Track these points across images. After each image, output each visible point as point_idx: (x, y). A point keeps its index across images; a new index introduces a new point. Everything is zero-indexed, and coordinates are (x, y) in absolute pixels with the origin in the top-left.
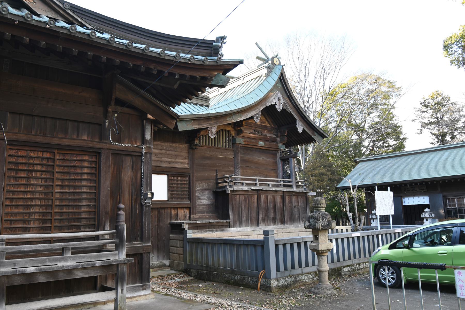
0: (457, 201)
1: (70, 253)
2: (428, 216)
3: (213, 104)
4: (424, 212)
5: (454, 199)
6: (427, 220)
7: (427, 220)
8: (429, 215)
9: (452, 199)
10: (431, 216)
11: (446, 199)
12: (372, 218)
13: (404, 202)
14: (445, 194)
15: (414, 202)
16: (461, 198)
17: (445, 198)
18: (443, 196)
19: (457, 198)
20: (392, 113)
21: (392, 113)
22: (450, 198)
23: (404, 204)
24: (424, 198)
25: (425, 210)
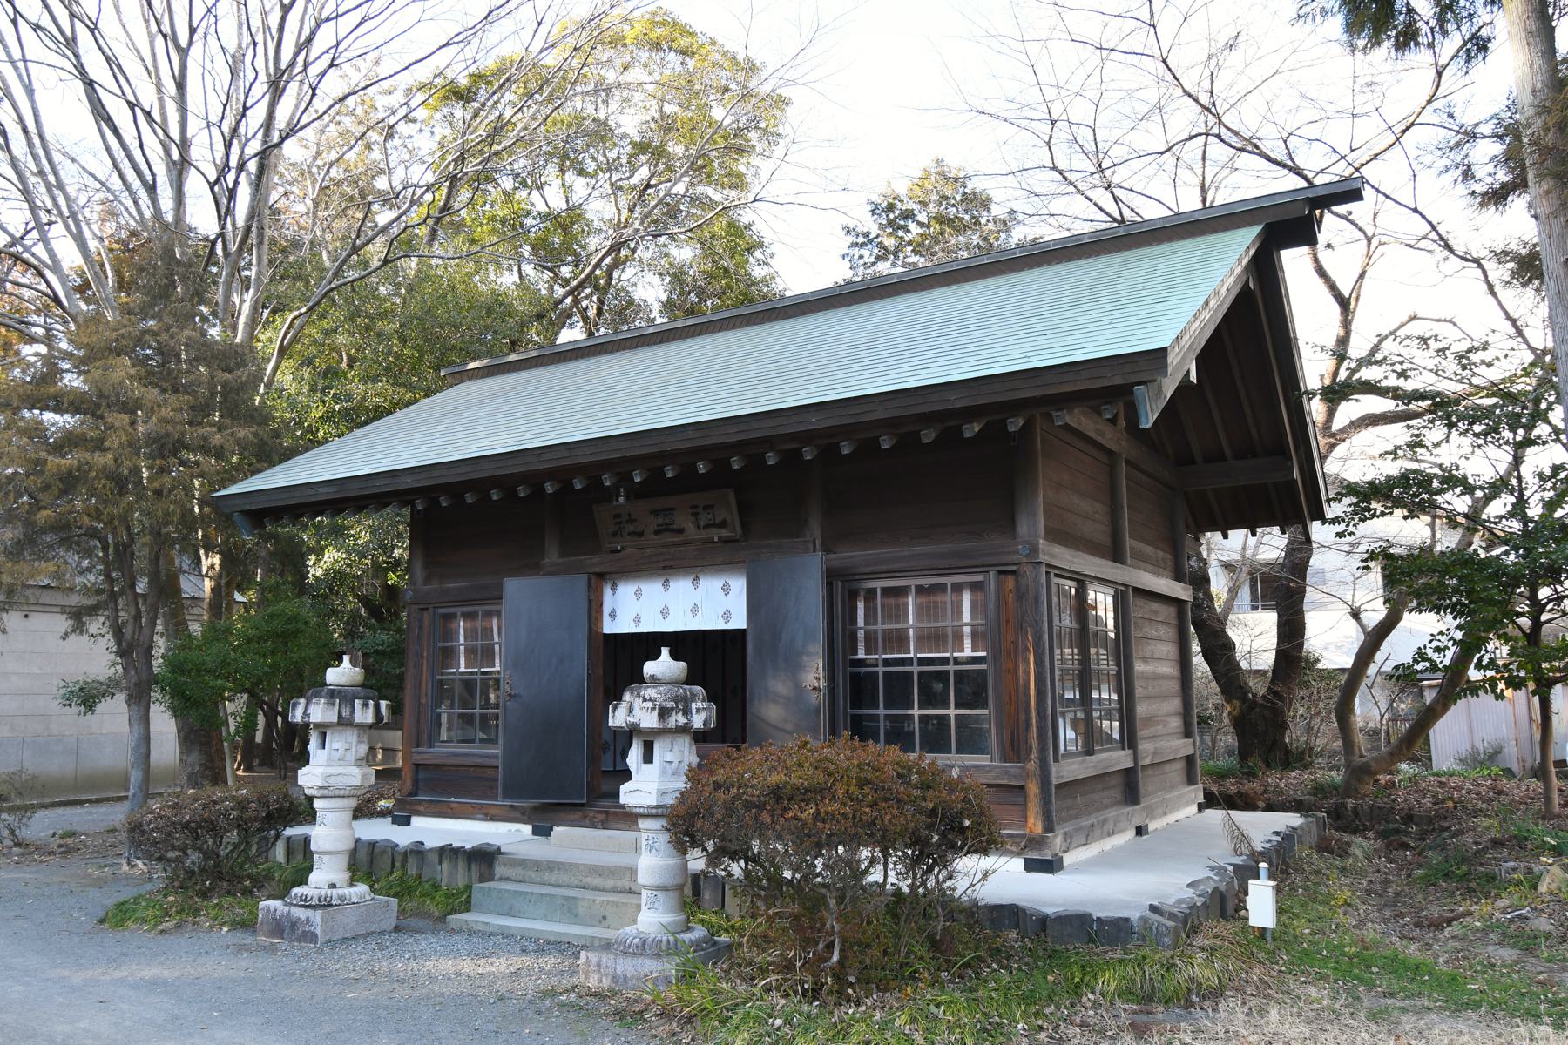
0: (917, 607)
1: (49, 466)
2: (649, 721)
3: (1079, 206)
4: (639, 679)
5: (901, 592)
6: (648, 758)
7: (648, 758)
8: (664, 713)
9: (887, 592)
10: (678, 719)
11: (853, 596)
12: (632, 732)
13: (613, 615)
14: (849, 556)
15: (665, 612)
16: (941, 588)
17: (843, 588)
18: (831, 576)
19: (921, 590)
20: (79, 618)
21: (79, 618)
22: (879, 584)
23: (609, 627)
24: (638, 594)
25: (649, 668)
